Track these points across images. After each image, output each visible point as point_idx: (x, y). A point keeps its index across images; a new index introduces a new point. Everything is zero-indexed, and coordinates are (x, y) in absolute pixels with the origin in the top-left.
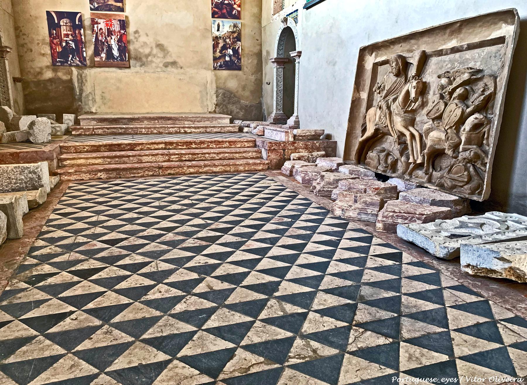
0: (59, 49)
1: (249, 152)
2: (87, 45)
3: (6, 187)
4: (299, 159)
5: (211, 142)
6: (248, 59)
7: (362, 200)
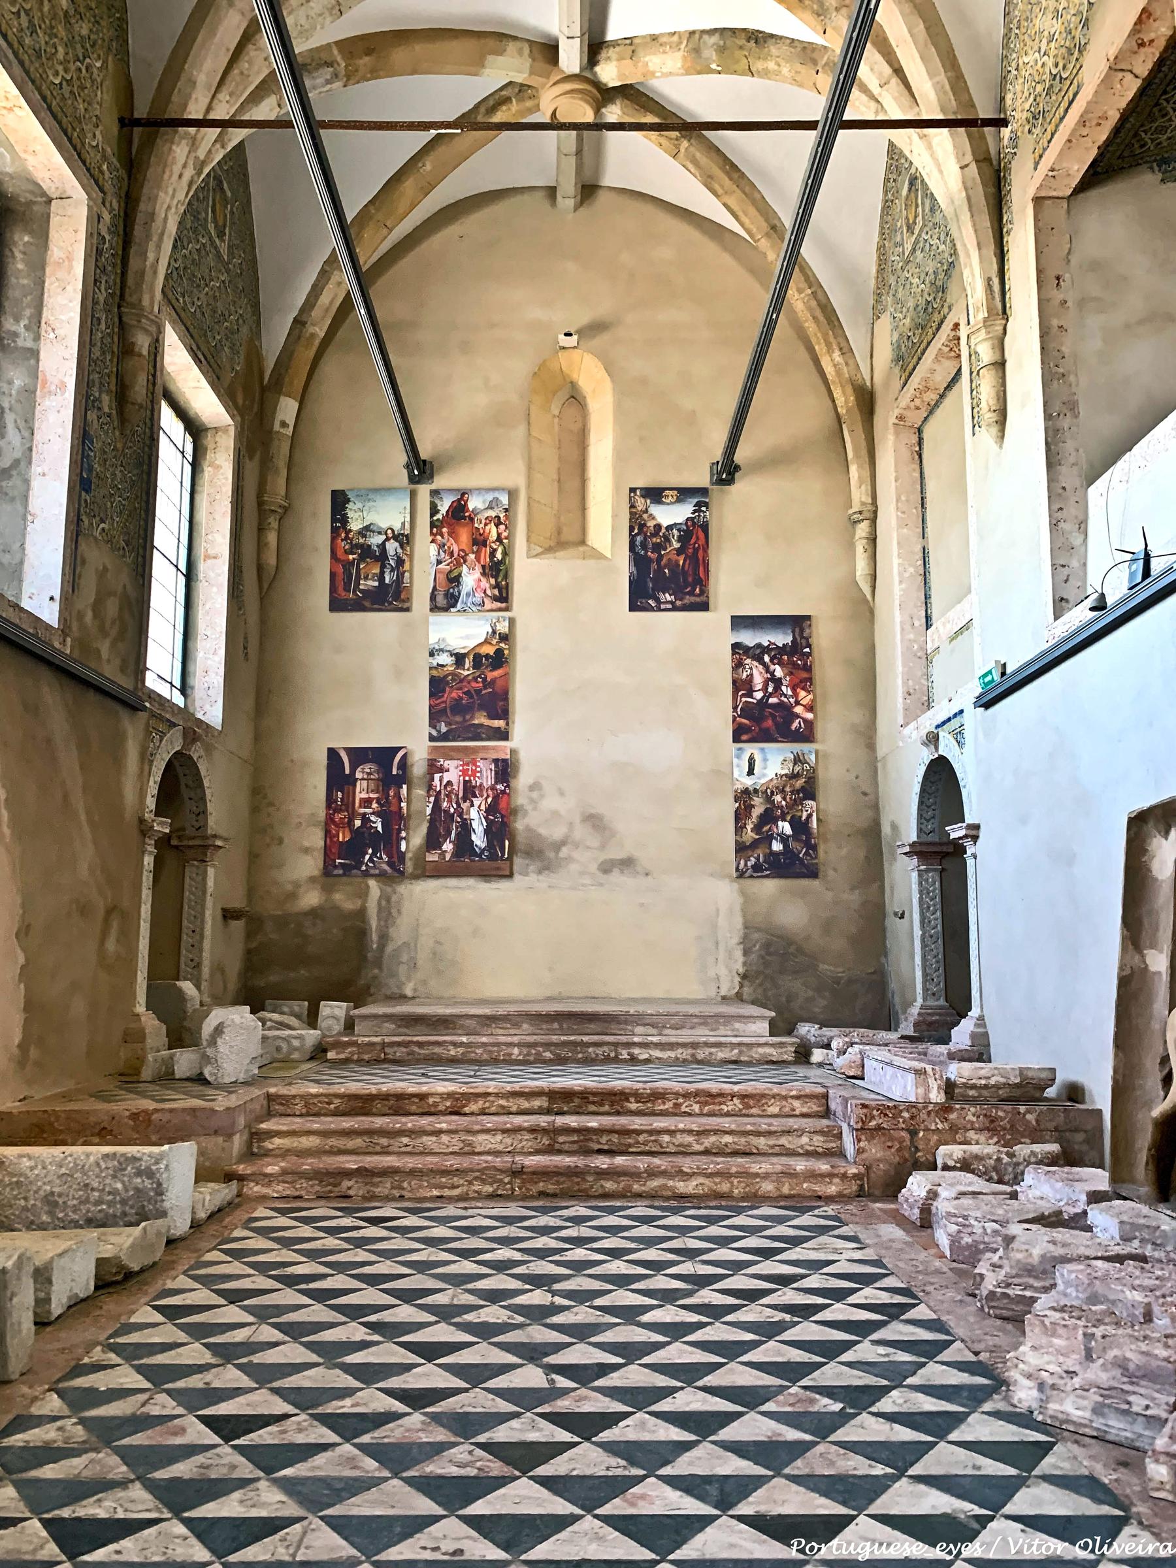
0: (343, 836)
1: (801, 1132)
2: (412, 823)
3: (74, 1212)
4: (965, 1166)
5: (686, 1095)
6: (840, 847)
7: (1112, 1354)
